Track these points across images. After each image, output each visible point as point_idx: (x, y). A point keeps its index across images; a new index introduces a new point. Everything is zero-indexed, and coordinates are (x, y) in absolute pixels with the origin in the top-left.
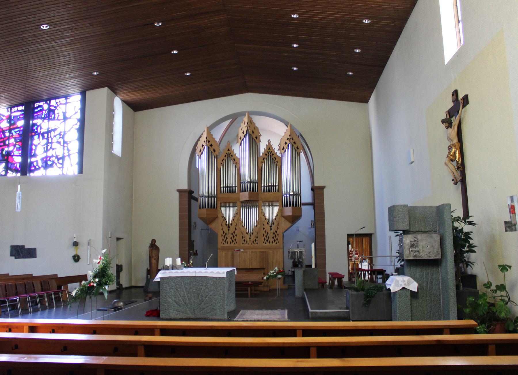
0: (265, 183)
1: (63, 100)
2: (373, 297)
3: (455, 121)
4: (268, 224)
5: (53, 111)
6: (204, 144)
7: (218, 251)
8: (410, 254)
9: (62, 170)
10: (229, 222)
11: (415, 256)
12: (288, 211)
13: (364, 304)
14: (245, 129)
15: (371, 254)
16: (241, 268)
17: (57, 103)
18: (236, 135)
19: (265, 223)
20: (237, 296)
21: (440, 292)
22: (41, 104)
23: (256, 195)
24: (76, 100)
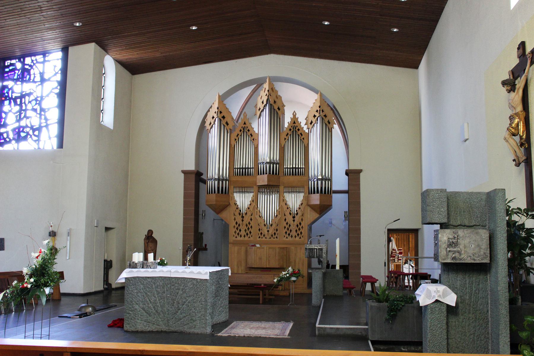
0: (288, 164)
1: (40, 58)
2: (399, 310)
3: (520, 83)
4: (290, 214)
5: (28, 71)
6: (215, 116)
7: (230, 245)
8: (447, 255)
9: (38, 144)
10: (243, 211)
11: (454, 258)
12: (316, 199)
13: (387, 320)
14: (265, 99)
15: (417, 254)
16: (256, 267)
17: (32, 61)
18: (255, 104)
19: (287, 213)
20: (230, 302)
21: (487, 307)
22: (13, 61)
23: (277, 179)
24: (55, 58)
